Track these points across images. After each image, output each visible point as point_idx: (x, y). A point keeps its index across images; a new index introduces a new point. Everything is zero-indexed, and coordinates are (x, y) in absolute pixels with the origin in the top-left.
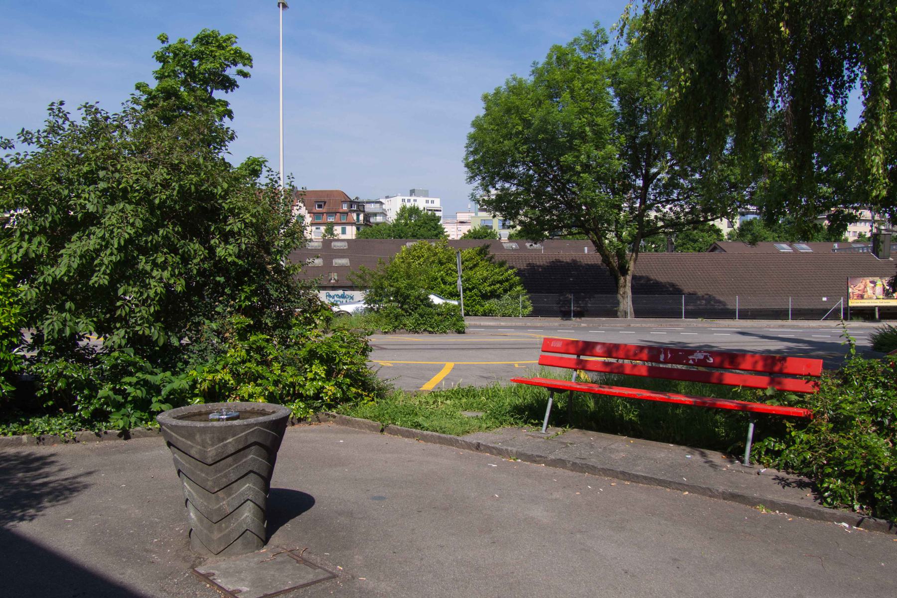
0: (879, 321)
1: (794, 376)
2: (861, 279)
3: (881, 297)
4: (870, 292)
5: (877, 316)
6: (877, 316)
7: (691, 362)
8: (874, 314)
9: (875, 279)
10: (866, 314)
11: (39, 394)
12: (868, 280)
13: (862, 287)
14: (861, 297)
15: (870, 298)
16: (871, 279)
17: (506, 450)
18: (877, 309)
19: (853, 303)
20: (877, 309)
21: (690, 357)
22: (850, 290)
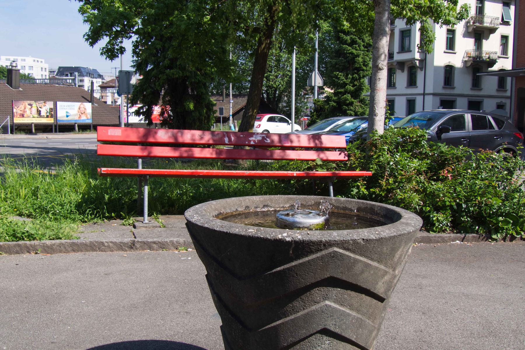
0: (35, 134)
1: (293, 148)
2: (22, 102)
3: (36, 116)
4: (28, 112)
5: (34, 131)
6: (34, 131)
7: (252, 143)
8: (32, 129)
9: (32, 102)
10: (26, 129)
11: (335, 104)
12: (27, 103)
13: (23, 108)
14: (23, 116)
15: (29, 117)
16: (29, 102)
17: (172, 242)
18: (76, 125)
19: (18, 120)
20: (76, 125)
21: (251, 139)
22: (15, 110)
